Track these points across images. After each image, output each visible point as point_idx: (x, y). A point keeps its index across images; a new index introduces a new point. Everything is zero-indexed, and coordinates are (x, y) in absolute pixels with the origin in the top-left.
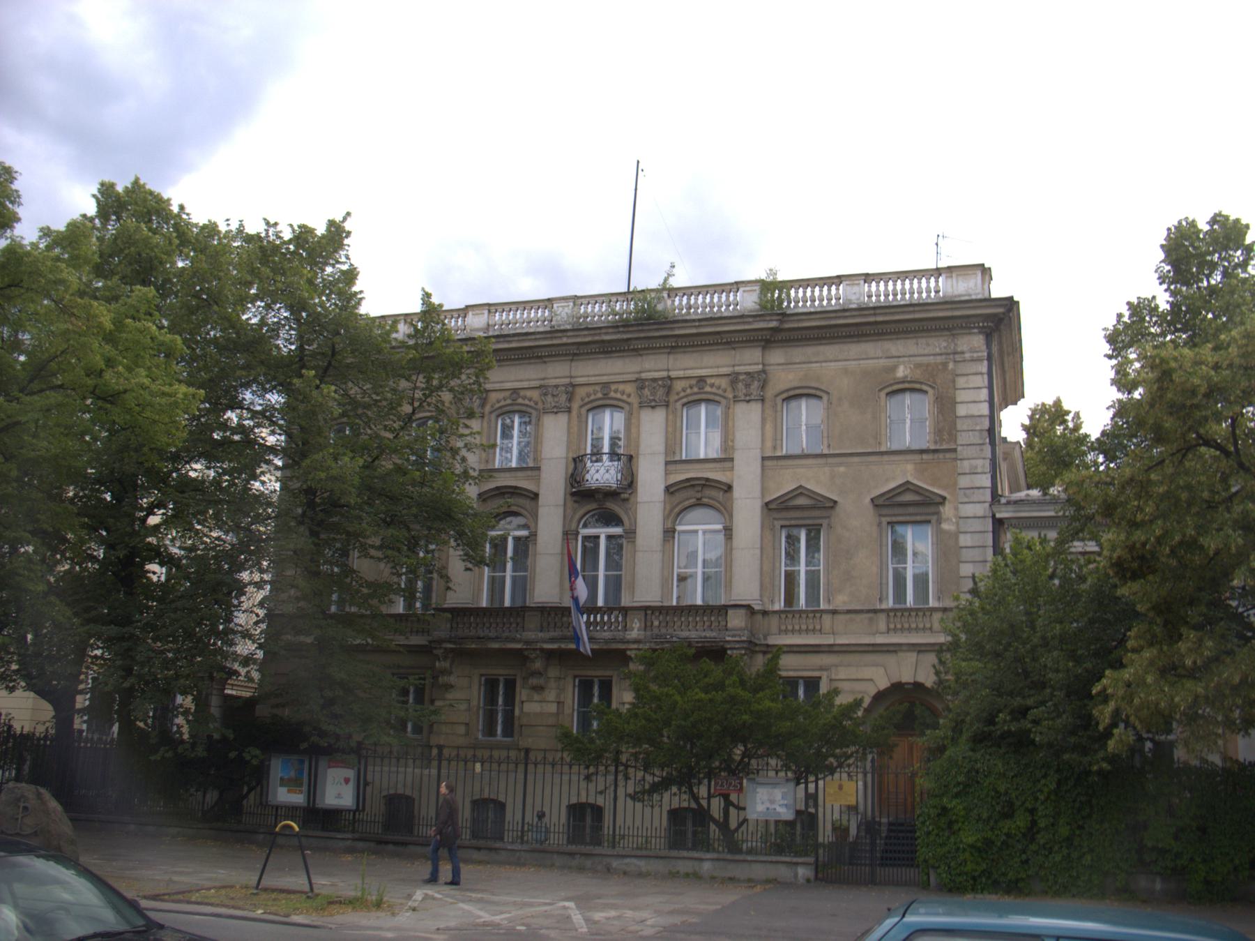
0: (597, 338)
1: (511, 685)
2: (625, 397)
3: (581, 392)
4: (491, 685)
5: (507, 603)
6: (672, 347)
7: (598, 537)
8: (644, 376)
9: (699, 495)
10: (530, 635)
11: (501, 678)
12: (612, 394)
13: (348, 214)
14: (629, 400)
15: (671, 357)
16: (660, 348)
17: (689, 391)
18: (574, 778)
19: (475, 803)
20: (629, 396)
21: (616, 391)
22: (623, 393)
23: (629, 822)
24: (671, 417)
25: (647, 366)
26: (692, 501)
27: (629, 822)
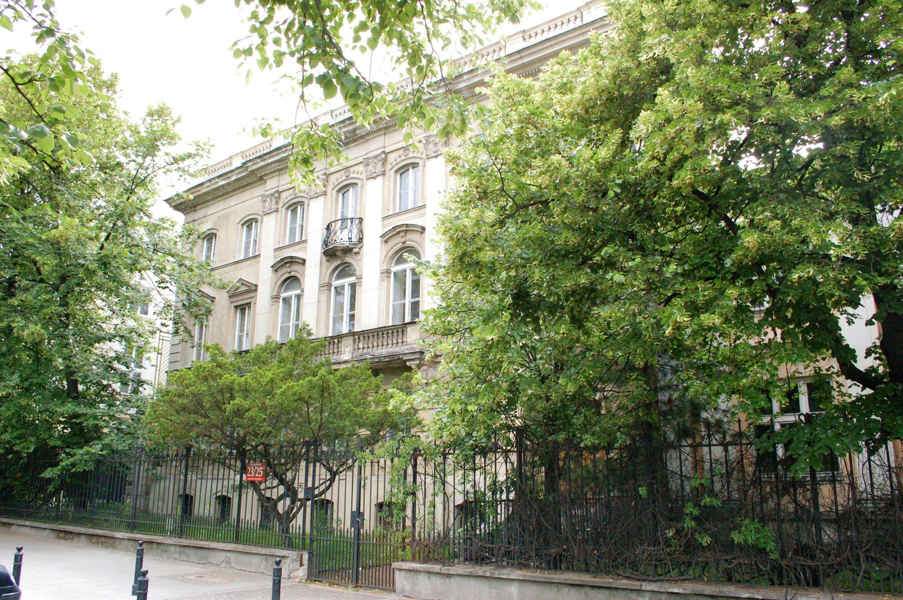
3: (391, 157)
6: (386, 128)
7: (343, 286)
8: (369, 155)
12: (352, 175)
13: (247, 82)
15: (387, 137)
16: (272, 172)
17: (399, 160)
19: (380, 506)
21: (353, 173)
23: (248, 517)
24: (386, 183)
25: (281, 183)
27: (248, 517)
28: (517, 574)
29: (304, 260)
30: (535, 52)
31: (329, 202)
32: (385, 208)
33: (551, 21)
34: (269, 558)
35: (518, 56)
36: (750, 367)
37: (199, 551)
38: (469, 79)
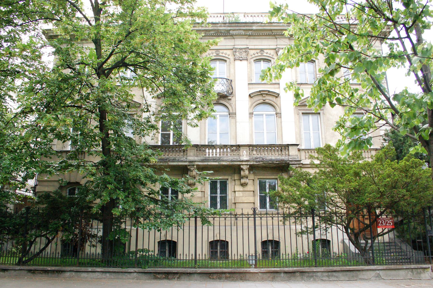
0: (216, 28)
1: (224, 185)
2: (227, 56)
4: (213, 185)
5: (171, 144)
6: (249, 35)
9: (264, 99)
10: (191, 158)
11: (219, 181)
12: (221, 54)
14: (229, 57)
17: (256, 55)
18: (228, 223)
20: (229, 55)
22: (226, 54)
26: (262, 101)
29: (279, 94)
30: (244, 26)
33: (257, 13)
34: (414, 270)
37: (348, 273)
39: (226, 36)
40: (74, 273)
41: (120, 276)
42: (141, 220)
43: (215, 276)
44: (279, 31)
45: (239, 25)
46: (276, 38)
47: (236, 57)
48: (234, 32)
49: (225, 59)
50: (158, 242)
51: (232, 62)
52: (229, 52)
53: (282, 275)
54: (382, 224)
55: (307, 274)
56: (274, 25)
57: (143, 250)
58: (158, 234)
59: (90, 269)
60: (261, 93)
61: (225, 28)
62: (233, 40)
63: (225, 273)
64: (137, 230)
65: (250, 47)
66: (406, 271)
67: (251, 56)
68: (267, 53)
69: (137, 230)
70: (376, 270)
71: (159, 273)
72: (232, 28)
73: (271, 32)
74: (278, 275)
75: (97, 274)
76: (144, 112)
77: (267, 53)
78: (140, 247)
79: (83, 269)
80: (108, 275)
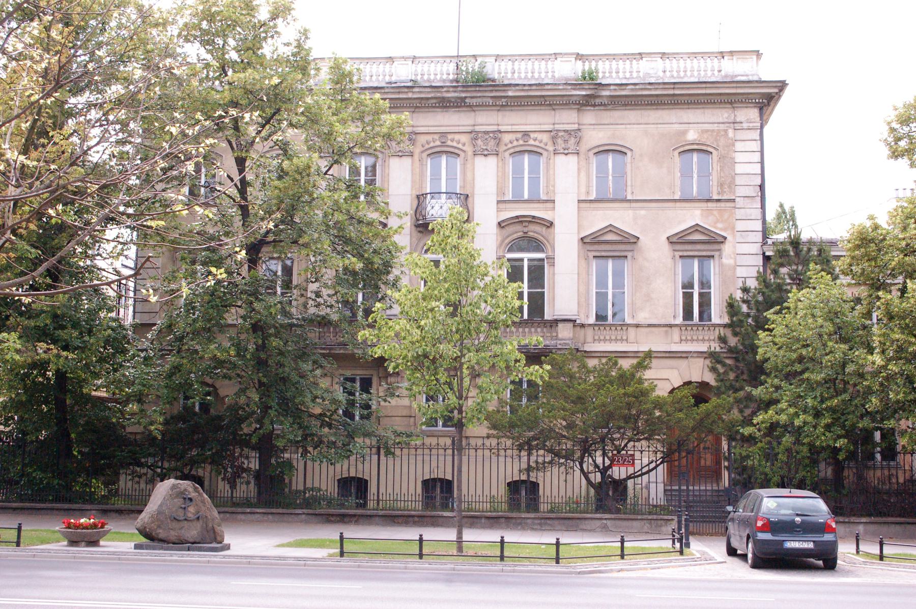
0: (439, 95)
2: (460, 146)
9: (526, 230)
12: (449, 143)
14: (464, 148)
17: (515, 143)
20: (464, 145)
21: (452, 140)
28: (864, 520)
30: (492, 91)
31: (417, 163)
32: (501, 190)
35: (672, 86)
36: (621, 408)
37: (566, 522)
38: (615, 90)
39: (459, 107)
40: (228, 515)
41: (286, 518)
42: (310, 449)
43: (400, 520)
44: (558, 98)
45: (481, 89)
46: (554, 110)
47: (477, 148)
48: (474, 101)
49: (456, 151)
50: (339, 480)
51: (469, 158)
52: (464, 138)
53: (483, 520)
54: (618, 461)
55: (514, 521)
56: (546, 87)
57: (312, 489)
58: (331, 468)
59: (248, 510)
60: (519, 220)
61: (456, 95)
62: (473, 114)
63: (413, 516)
64: (305, 463)
65: (503, 128)
66: (643, 522)
67: (506, 145)
68: (535, 140)
69: (305, 463)
70: (601, 519)
71: (333, 515)
72: (468, 95)
73: (542, 99)
74: (478, 520)
75: (257, 516)
76: (312, 282)
77: (535, 140)
78: (309, 485)
79: (240, 510)
80: (270, 517)
